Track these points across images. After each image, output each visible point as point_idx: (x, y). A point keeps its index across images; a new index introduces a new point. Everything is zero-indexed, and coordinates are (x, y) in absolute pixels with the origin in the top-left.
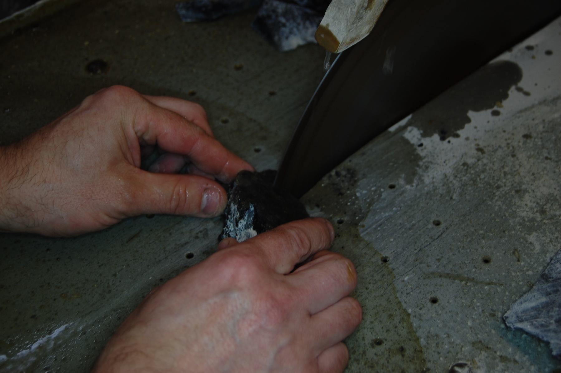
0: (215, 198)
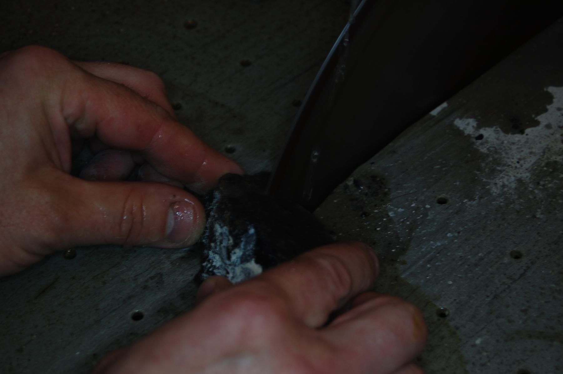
0: (187, 216)
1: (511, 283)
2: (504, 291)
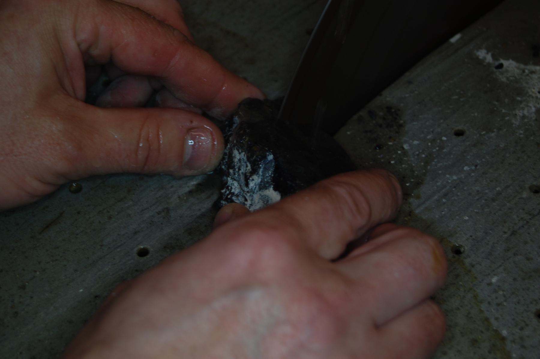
0: (204, 142)
1: (530, 219)
2: (523, 227)
